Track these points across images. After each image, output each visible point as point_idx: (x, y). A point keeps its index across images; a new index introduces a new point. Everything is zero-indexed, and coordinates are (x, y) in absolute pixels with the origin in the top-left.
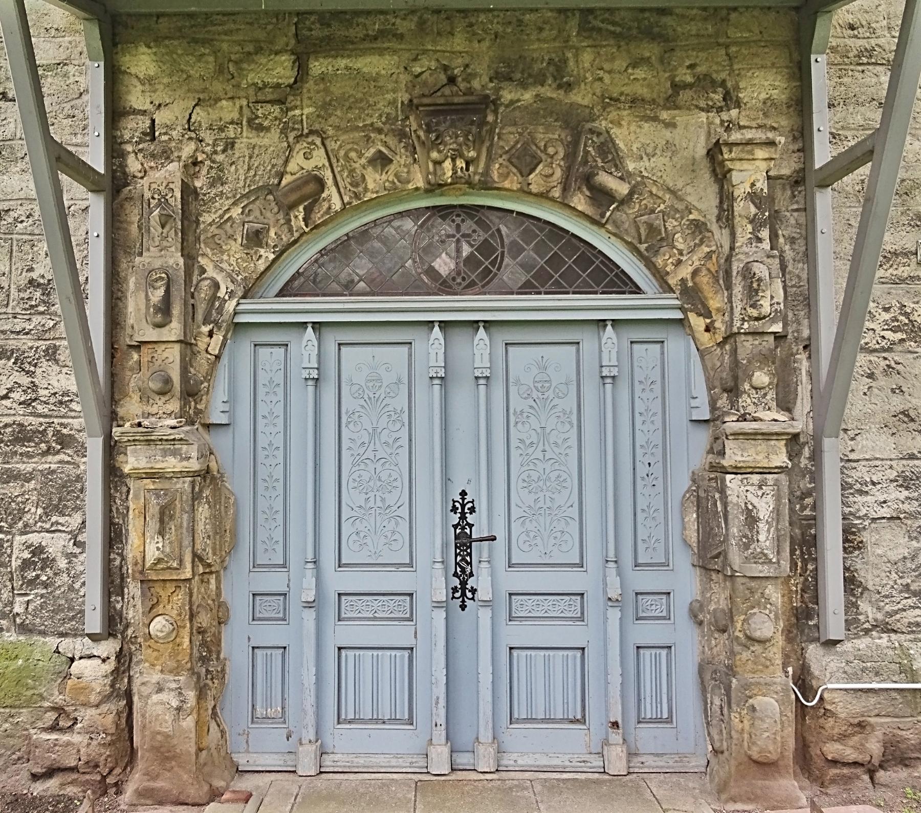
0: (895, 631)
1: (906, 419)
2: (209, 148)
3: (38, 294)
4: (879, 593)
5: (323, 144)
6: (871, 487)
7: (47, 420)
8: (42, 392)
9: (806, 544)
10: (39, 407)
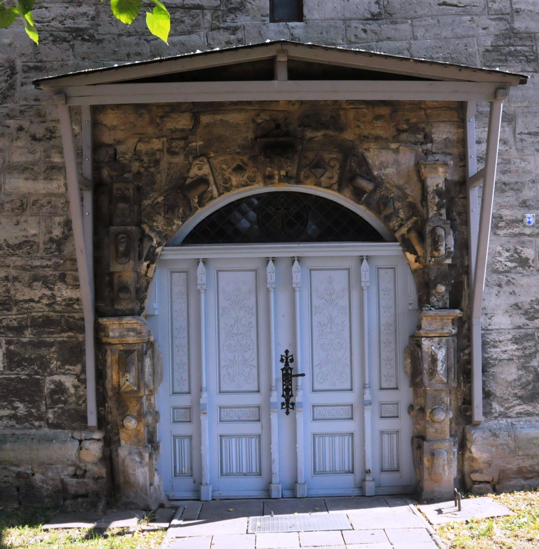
0: (510, 417)
1: (517, 308)
2: (146, 165)
3: (54, 246)
4: (502, 398)
5: (209, 162)
6: (499, 343)
7: (61, 314)
8: (59, 299)
9: (464, 372)
10: (57, 307)
